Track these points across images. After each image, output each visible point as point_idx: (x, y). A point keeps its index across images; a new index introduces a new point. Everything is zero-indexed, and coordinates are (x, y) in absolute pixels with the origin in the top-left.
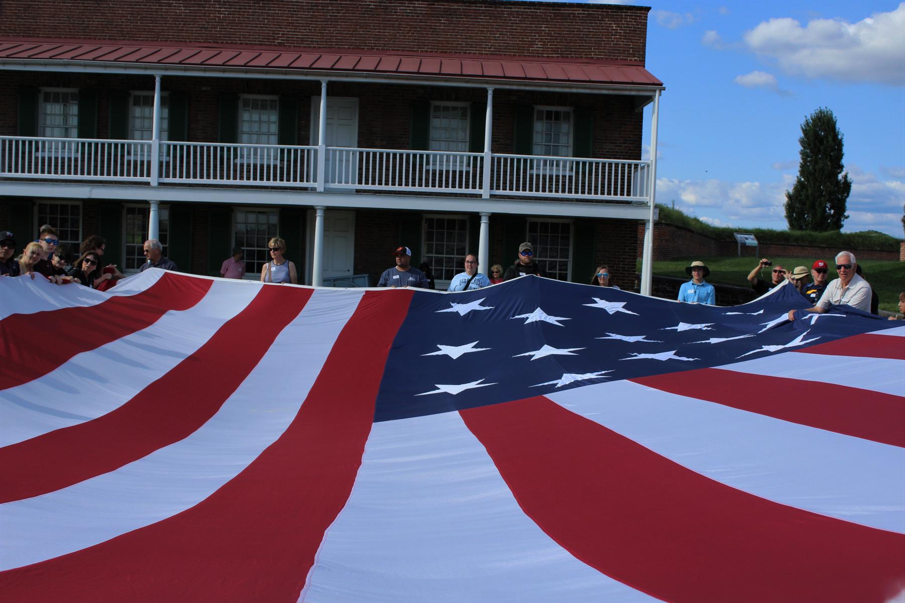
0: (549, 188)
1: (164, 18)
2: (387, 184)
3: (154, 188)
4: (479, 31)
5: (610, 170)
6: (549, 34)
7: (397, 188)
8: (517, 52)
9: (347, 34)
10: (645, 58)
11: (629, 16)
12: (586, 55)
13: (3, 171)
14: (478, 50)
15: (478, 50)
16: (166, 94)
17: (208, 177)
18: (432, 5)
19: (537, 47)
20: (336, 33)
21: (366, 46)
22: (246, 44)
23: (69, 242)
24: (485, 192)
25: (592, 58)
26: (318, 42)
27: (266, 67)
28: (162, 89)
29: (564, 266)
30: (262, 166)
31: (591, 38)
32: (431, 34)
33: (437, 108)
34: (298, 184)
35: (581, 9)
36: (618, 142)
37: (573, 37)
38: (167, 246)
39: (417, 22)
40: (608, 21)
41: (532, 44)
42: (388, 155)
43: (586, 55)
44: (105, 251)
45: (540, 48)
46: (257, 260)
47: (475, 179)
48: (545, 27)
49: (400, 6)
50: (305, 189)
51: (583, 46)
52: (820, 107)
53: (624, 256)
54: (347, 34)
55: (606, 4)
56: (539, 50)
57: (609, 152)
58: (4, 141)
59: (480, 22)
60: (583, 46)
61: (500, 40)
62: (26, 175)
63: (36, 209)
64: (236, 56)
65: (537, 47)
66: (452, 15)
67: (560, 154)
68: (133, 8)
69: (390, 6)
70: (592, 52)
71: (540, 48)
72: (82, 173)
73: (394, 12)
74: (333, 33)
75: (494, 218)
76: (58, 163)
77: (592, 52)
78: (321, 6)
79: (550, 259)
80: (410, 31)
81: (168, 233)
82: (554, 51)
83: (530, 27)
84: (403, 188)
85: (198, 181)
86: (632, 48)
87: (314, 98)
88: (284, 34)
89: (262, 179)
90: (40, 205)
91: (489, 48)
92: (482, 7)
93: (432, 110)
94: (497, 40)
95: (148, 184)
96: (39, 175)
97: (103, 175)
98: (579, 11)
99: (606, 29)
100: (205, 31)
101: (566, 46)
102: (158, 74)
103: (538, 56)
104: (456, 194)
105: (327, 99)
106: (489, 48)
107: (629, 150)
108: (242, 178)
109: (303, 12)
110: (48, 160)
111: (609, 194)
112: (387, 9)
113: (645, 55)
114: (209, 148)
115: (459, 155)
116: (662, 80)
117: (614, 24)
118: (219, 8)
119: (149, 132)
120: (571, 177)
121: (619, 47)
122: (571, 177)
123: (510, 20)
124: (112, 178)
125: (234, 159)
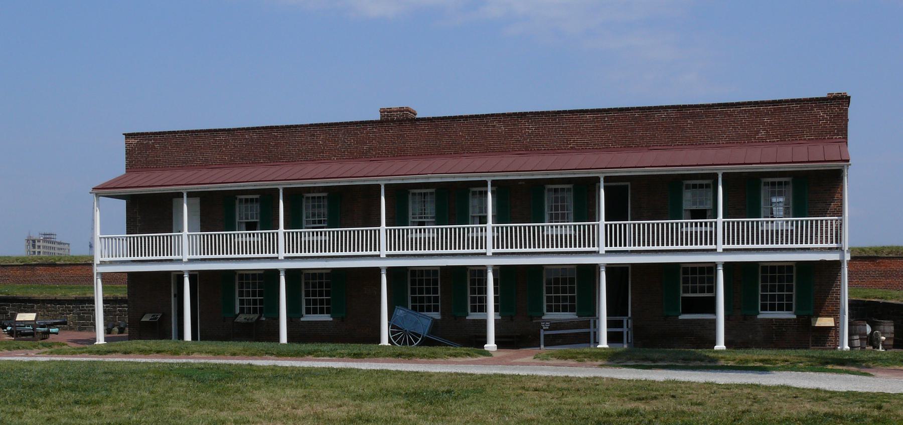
0: (781, 242)
1: (491, 136)
3: (383, 258)
4: (716, 126)
5: (817, 225)
6: (770, 124)
7: (703, 247)
8: (747, 140)
9: (620, 137)
10: (847, 135)
11: (423, 125)
12: (800, 137)
14: (717, 141)
15: (717, 141)
16: (494, 189)
17: (663, 245)
18: (681, 110)
19: (761, 135)
20: (612, 137)
21: (634, 144)
22: (548, 150)
25: (805, 139)
26: (598, 144)
28: (492, 186)
29: (789, 298)
31: (803, 124)
32: (681, 132)
33: (474, 193)
35: (794, 103)
36: (828, 201)
37: (789, 125)
38: (499, 295)
39: (670, 124)
40: (816, 110)
41: (758, 132)
43: (800, 137)
44: (442, 313)
45: (764, 135)
46: (310, 305)
47: (712, 239)
48: (767, 120)
49: (657, 114)
50: (171, 260)
51: (797, 131)
53: (837, 288)
54: (620, 137)
55: (722, 103)
56: (763, 137)
57: (821, 209)
59: (717, 120)
60: (797, 131)
61: (733, 132)
62: (741, 246)
63: (237, 277)
65: (761, 135)
66: (696, 116)
68: (470, 131)
69: (650, 114)
70: (805, 135)
71: (764, 135)
72: (777, 243)
73: (653, 118)
74: (609, 137)
76: (803, 235)
77: (805, 135)
78: (600, 119)
79: (779, 293)
80: (666, 130)
81: (576, 286)
82: (775, 136)
83: (756, 120)
86: (836, 129)
87: (597, 184)
88: (575, 141)
89: (687, 244)
90: (684, 268)
91: (725, 139)
92: (718, 109)
93: (470, 194)
94: (731, 132)
96: (750, 246)
97: (773, 244)
98: (793, 104)
99: (815, 117)
100: (519, 142)
101: (784, 132)
103: (763, 142)
104: (741, 249)
105: (187, 200)
106: (725, 139)
107: (837, 207)
109: (588, 123)
110: (556, 236)
111: (801, 243)
112: (648, 116)
113: (847, 133)
115: (709, 221)
117: (822, 112)
118: (528, 125)
119: (569, 216)
120: (792, 231)
121: (826, 129)
122: (792, 231)
123: (739, 116)
125: (681, 229)
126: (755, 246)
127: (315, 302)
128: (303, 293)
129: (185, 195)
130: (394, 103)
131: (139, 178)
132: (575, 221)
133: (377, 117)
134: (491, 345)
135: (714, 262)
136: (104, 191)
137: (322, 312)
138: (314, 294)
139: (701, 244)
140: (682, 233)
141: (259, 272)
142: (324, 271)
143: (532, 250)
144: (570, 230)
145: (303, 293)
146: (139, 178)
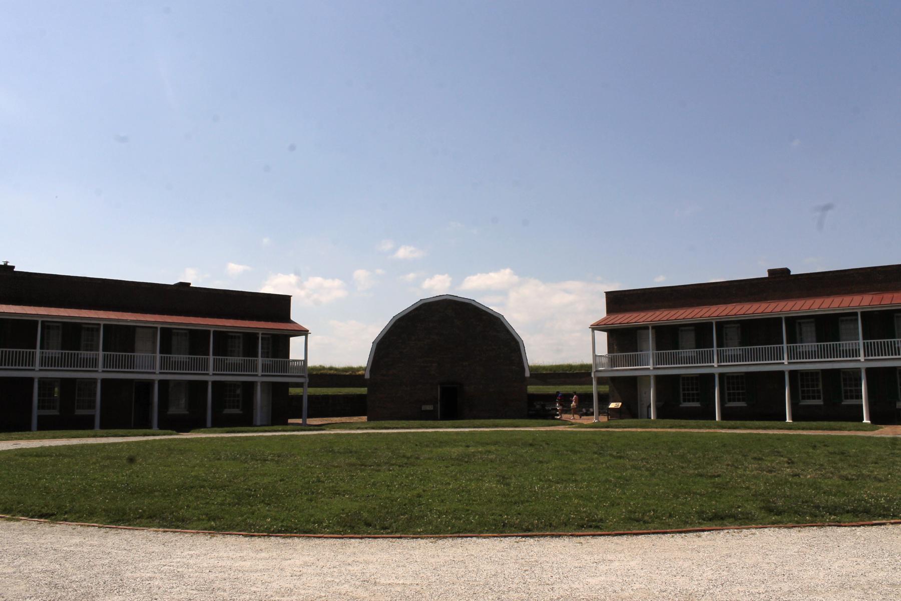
2: (131, 368)
13: (2, 365)
23: (695, 392)
24: (715, 364)
27: (771, 312)
30: (849, 350)
34: (132, 370)
42: (765, 348)
44: (824, 400)
52: (310, 333)
58: (2, 352)
64: (795, 304)
67: (639, 349)
75: (214, 383)
84: (126, 370)
85: (826, 360)
95: (859, 360)
102: (859, 311)
108: (828, 358)
114: (874, 343)
116: (306, 327)
124: (176, 371)
126: (187, 372)
127: (689, 395)
128: (681, 390)
129: (650, 327)
130: (788, 267)
131: (625, 318)
132: (244, 357)
133: (766, 275)
134: (788, 420)
135: (859, 368)
136: (596, 327)
137: (693, 401)
138: (688, 390)
139: (167, 369)
140: (840, 351)
141: (741, 374)
142: (739, 374)
143: (195, 372)
144: (694, 354)
145: (681, 390)
146: (625, 318)
